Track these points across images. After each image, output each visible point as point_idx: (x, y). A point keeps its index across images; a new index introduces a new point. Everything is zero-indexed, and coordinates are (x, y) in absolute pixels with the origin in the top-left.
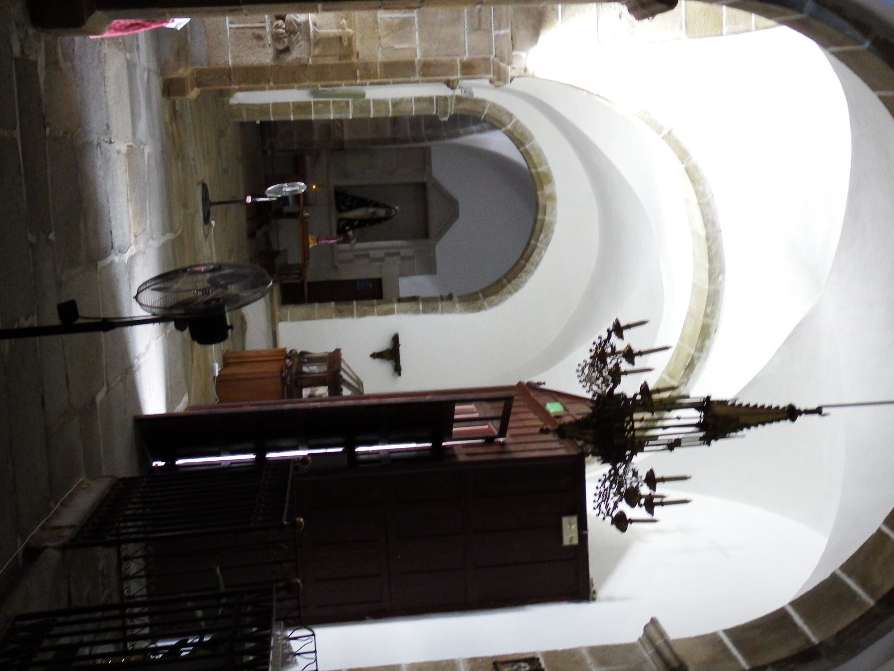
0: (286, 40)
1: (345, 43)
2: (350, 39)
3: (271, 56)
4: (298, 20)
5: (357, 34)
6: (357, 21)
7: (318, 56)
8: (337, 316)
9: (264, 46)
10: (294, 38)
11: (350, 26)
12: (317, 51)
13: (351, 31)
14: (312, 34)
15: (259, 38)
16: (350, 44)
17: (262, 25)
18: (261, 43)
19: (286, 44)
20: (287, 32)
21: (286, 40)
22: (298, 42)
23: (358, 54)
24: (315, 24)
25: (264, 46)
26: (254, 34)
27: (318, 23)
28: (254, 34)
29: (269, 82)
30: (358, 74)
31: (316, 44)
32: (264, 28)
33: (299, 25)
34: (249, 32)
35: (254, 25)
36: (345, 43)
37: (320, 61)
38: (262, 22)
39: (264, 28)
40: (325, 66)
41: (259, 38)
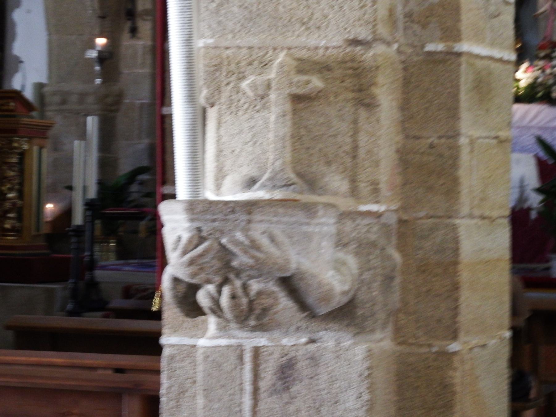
0: (255, 286)
1: (316, 83)
2: (305, 66)
3: (347, 343)
4: (186, 236)
5: (290, 41)
6: (254, 41)
7: (353, 181)
8: (99, 180)
9: (314, 360)
10: (241, 260)
11: (265, 65)
12: (337, 182)
13: (281, 56)
14: (278, 195)
15: (287, 371)
16: (323, 68)
17: (248, 357)
18: (302, 365)
19: (273, 287)
20: (226, 281)
21: (255, 286)
22: (255, 245)
23: (355, 42)
24: (251, 183)
25: (314, 360)
26: (274, 391)
27: (247, 171)
28: (274, 391)
29: (447, 357)
30: (440, 47)
31: (311, 183)
32: (257, 352)
33: (199, 238)
34: (267, 403)
35: (248, 387)
36: (316, 83)
37: (385, 170)
38: (241, 358)
39: (257, 352)
40: (405, 160)
41: (287, 371)
